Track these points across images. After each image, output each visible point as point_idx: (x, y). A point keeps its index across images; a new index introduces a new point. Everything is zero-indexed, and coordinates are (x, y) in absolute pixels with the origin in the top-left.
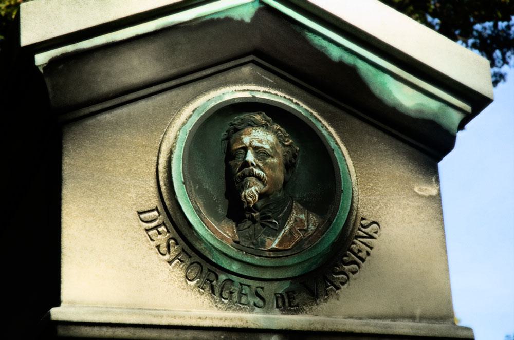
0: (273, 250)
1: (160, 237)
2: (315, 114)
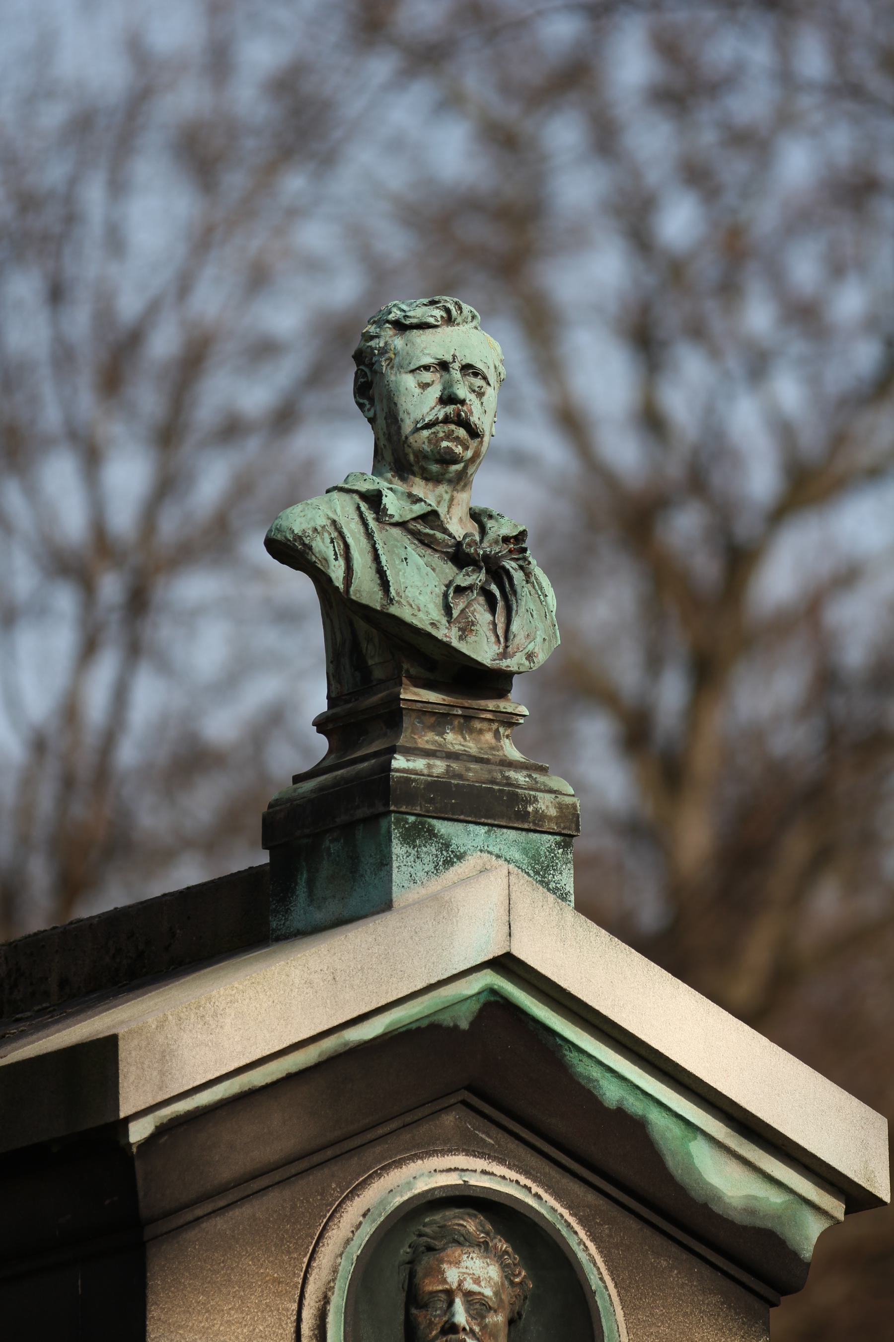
2: (572, 1220)
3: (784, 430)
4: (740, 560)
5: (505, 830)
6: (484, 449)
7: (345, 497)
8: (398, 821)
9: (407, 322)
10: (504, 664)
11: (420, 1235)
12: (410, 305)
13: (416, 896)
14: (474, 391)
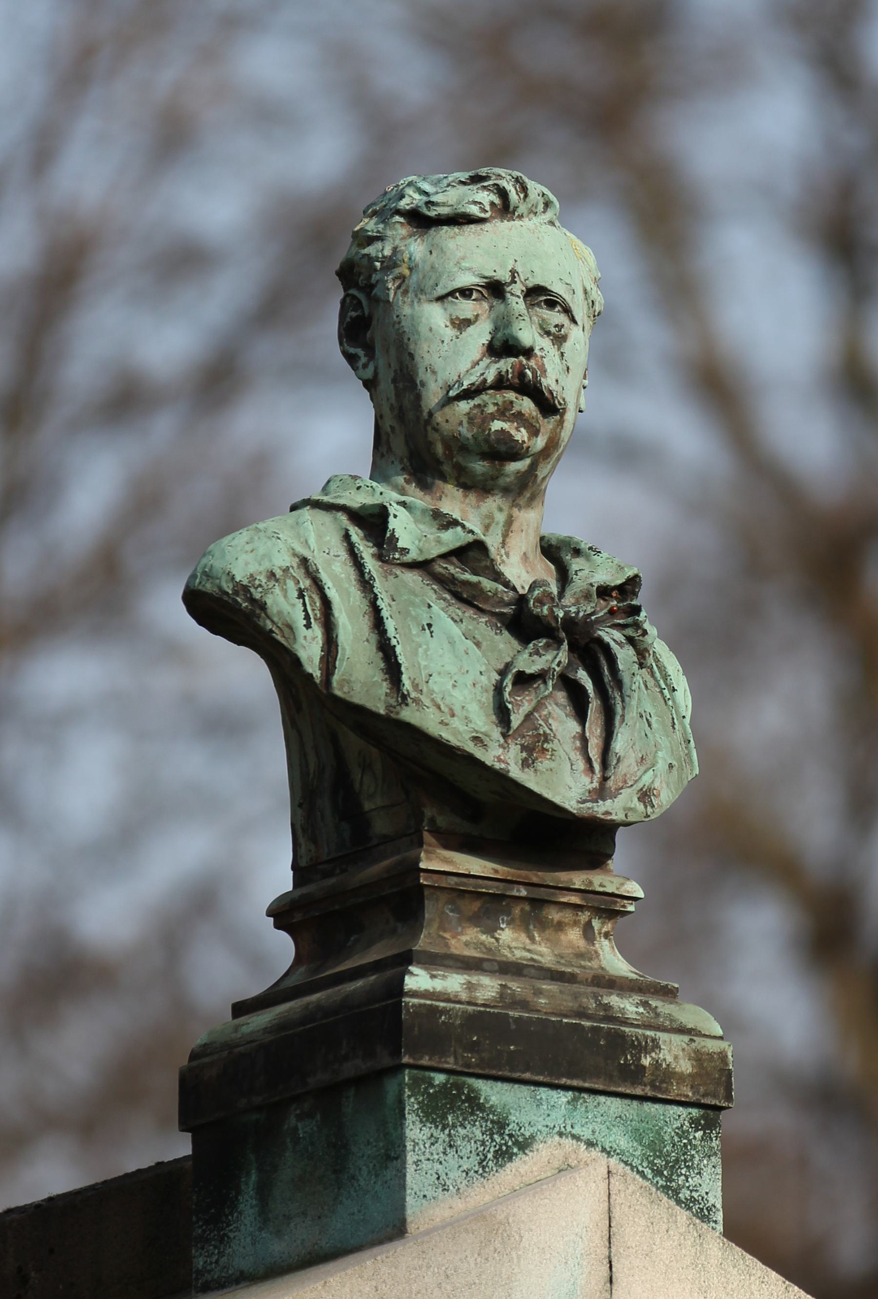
5: (602, 1099)
8: (416, 1083)
10: (600, 809)
13: (447, 1213)
14: (548, 333)
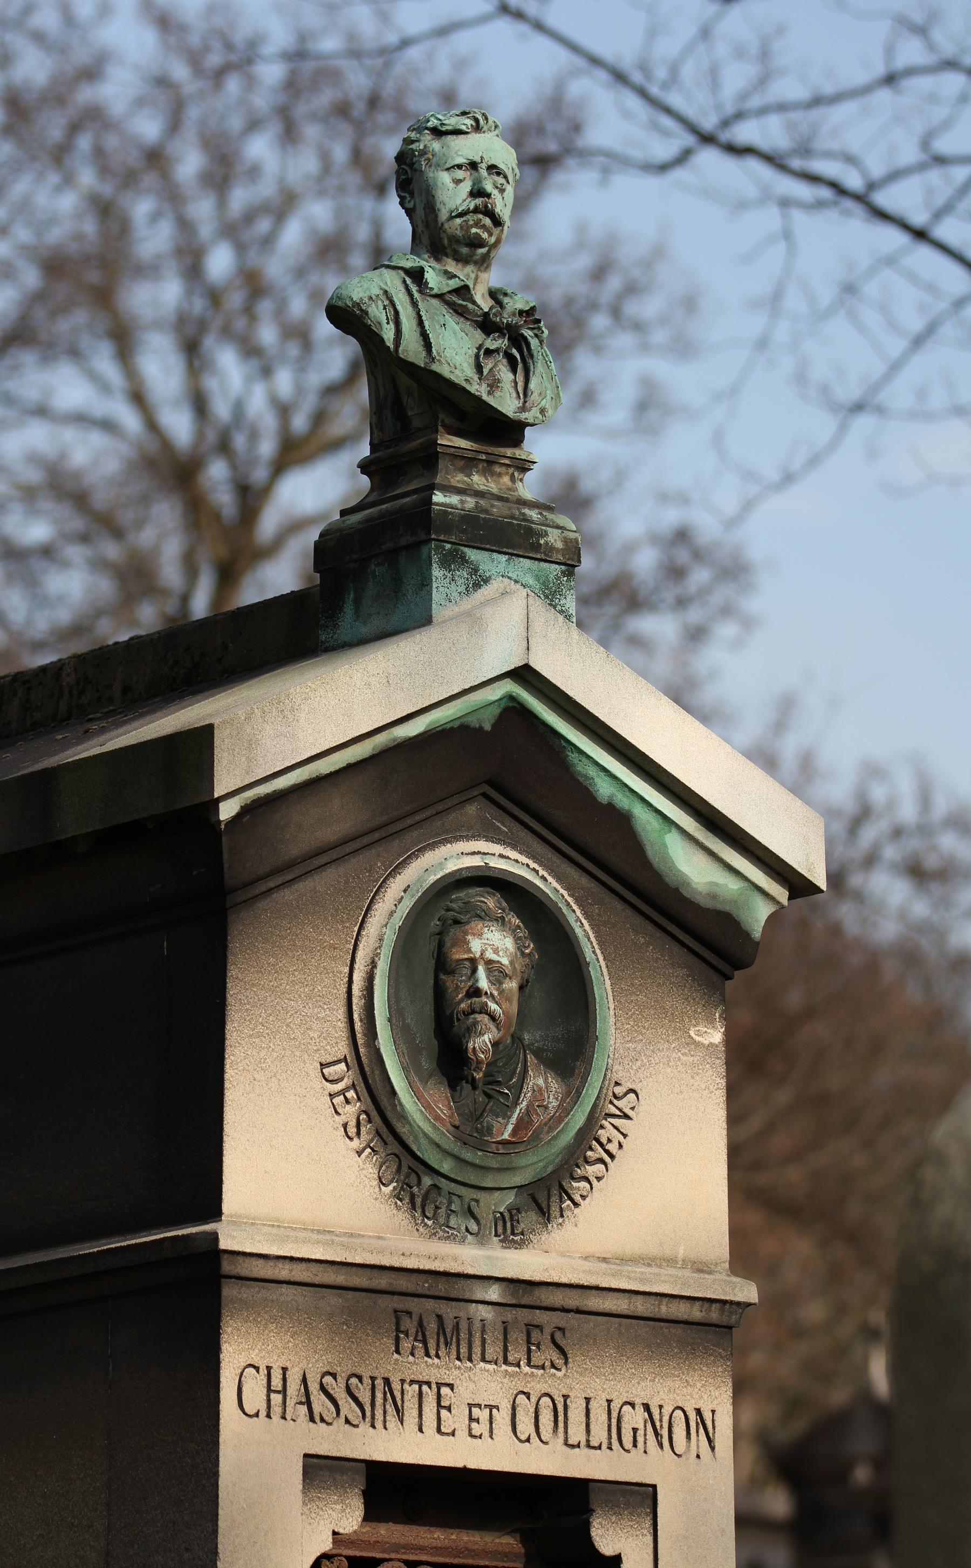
0: (505, 1143)
1: (348, 1107)
3: (284, 410)
4: (251, 498)
5: (521, 559)
6: (504, 236)
7: (393, 273)
8: (437, 548)
9: (443, 129)
10: (523, 416)
11: (448, 910)
12: (445, 115)
13: (451, 613)
14: (497, 187)
